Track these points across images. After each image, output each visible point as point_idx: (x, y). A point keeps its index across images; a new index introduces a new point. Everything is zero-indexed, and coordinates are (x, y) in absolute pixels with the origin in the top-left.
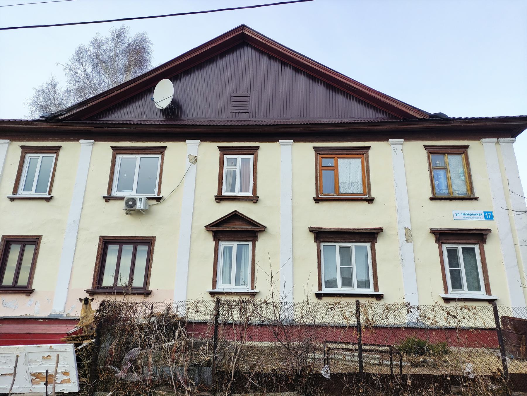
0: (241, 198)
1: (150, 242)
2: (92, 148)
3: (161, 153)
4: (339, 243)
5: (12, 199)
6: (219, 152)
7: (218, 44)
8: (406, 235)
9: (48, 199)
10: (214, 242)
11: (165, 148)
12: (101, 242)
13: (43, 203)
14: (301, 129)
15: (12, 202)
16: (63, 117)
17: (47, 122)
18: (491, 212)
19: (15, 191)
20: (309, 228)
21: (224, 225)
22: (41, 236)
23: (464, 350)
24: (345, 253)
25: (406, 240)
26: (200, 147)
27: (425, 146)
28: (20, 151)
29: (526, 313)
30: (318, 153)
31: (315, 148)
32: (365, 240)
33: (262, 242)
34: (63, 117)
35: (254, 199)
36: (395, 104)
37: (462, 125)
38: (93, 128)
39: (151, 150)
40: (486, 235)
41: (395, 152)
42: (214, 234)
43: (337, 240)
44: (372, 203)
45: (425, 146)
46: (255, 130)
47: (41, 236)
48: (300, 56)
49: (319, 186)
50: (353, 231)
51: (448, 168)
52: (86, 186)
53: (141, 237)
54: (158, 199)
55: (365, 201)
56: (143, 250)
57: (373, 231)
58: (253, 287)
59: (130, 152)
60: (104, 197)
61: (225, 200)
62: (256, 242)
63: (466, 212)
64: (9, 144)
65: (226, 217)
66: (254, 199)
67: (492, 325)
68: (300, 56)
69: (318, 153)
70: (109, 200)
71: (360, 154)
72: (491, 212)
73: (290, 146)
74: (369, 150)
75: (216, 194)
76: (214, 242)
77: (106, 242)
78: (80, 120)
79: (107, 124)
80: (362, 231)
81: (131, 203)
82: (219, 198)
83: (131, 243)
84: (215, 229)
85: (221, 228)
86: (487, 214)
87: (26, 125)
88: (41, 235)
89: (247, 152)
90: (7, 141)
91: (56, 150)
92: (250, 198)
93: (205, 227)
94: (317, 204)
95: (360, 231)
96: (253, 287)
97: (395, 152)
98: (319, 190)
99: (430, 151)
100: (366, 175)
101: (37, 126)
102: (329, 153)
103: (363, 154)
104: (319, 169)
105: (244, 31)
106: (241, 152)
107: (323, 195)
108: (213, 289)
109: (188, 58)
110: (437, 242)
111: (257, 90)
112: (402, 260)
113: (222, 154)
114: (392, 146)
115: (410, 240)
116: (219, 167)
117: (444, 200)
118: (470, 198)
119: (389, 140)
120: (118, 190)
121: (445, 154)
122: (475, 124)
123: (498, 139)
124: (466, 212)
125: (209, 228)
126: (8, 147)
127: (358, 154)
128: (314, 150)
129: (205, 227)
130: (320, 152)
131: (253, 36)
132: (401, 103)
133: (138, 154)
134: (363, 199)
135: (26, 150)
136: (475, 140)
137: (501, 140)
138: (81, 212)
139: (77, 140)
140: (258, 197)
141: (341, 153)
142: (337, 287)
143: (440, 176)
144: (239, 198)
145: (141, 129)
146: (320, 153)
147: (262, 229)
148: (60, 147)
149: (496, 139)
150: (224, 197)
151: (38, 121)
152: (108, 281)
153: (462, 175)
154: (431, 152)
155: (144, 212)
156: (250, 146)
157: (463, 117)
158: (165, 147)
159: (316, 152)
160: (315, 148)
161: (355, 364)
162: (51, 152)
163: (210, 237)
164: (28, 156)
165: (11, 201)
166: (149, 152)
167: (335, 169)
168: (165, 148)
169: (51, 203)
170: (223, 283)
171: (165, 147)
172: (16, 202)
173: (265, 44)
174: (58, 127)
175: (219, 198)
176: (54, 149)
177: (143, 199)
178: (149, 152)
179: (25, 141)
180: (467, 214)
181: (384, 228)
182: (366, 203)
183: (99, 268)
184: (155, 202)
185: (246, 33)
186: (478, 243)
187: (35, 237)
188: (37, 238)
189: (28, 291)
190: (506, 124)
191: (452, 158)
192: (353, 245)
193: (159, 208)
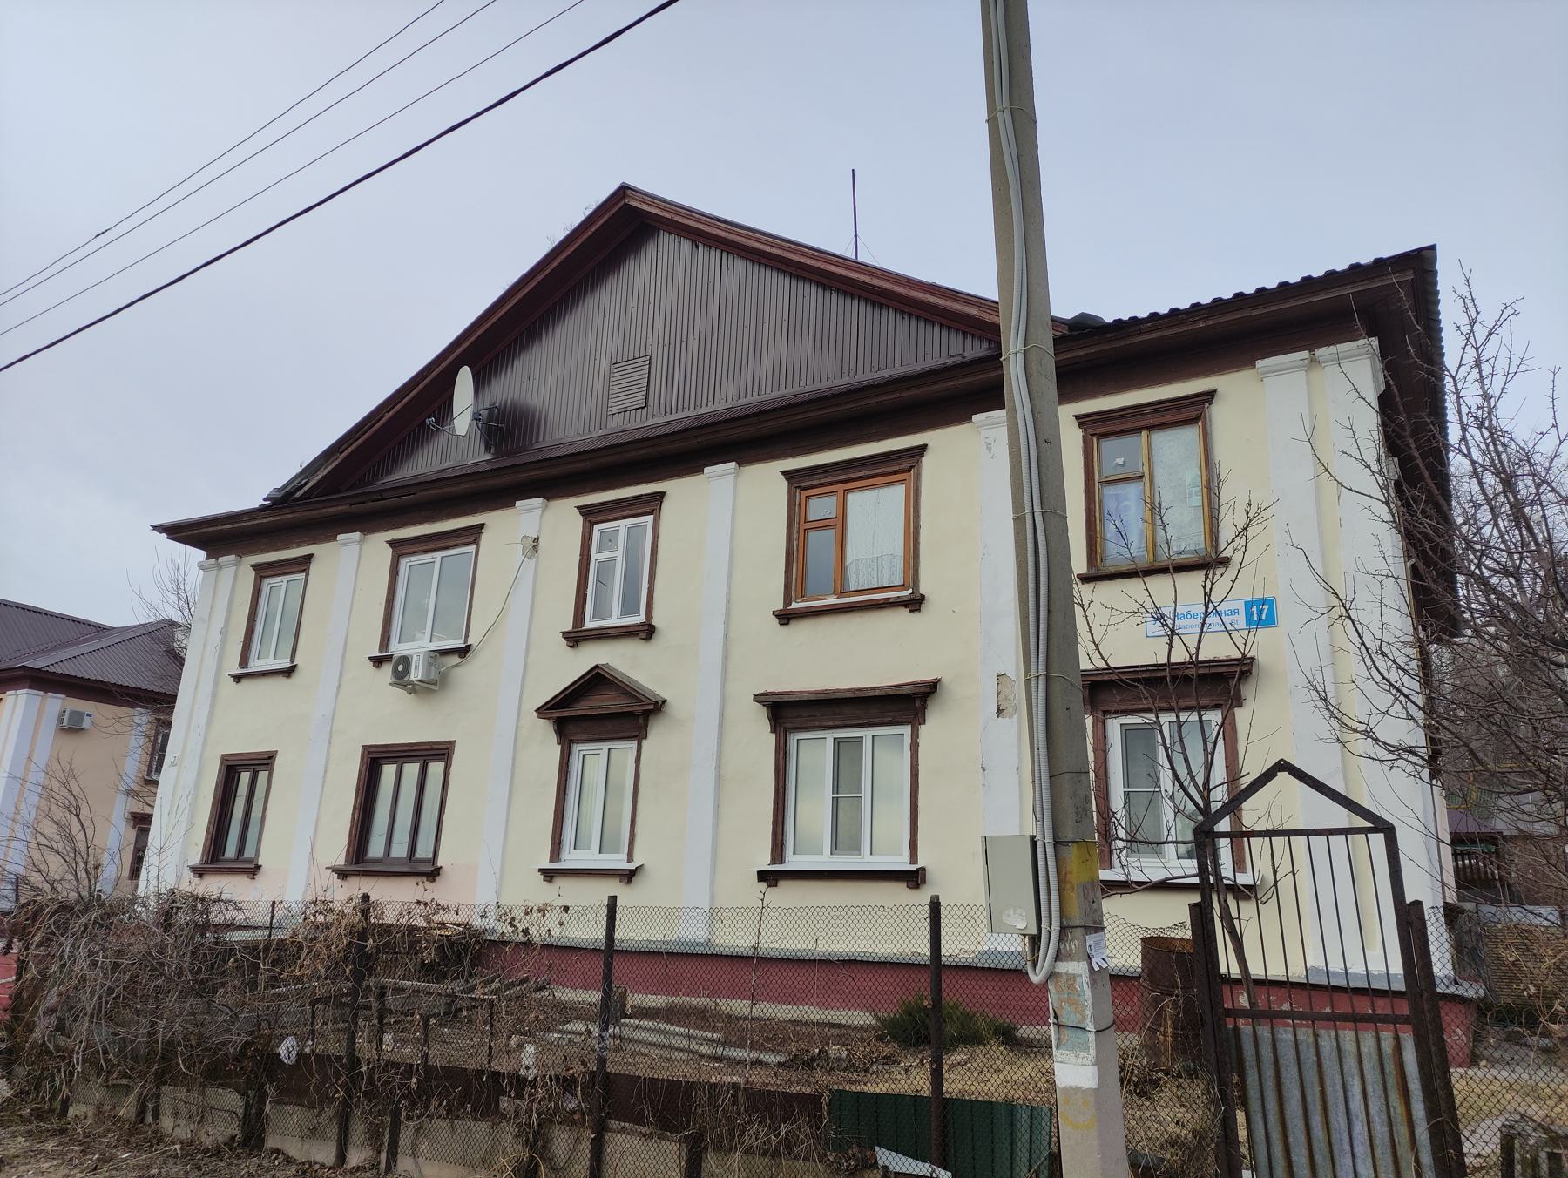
0: (613, 631)
1: (444, 754)
2: (360, 550)
3: (304, 571)
4: (834, 731)
5: (238, 678)
6: (581, 518)
8: (999, 694)
9: (289, 672)
10: (560, 746)
11: (660, 496)
12: (365, 759)
13: (281, 681)
14: (464, 487)
16: (301, 492)
17: (277, 509)
18: (1270, 602)
19: (244, 662)
21: (579, 702)
22: (275, 753)
24: (846, 762)
25: (1000, 712)
26: (546, 513)
27: (784, 473)
28: (579, 520)
30: (799, 487)
32: (894, 718)
33: (658, 737)
34: (301, 492)
35: (647, 631)
36: (973, 311)
37: (1171, 332)
38: (348, 507)
39: (456, 537)
41: (989, 450)
43: (825, 724)
44: (919, 610)
45: (784, 473)
46: (642, 452)
47: (275, 753)
48: (741, 231)
49: (794, 576)
50: (856, 696)
51: (1147, 474)
52: (347, 636)
53: (429, 743)
54: (464, 652)
55: (902, 605)
56: (436, 769)
57: (906, 691)
58: (914, 858)
59: (421, 549)
61: (802, 617)
62: (644, 741)
63: (1188, 608)
64: (361, 542)
65: (574, 688)
66: (647, 631)
67: (1130, 961)
68: (741, 231)
69: (796, 485)
70: (381, 663)
71: (902, 471)
72: (1270, 602)
74: (922, 455)
76: (560, 746)
77: (373, 760)
78: (340, 492)
79: (381, 494)
80: (877, 693)
81: (401, 668)
82: (576, 638)
83: (412, 758)
84: (557, 714)
85: (566, 713)
86: (1254, 609)
87: (249, 521)
88: (449, 742)
89: (639, 511)
90: (232, 557)
91: (1193, 411)
92: (631, 629)
93: (536, 711)
94: (785, 629)
95: (871, 694)
96: (914, 858)
97: (989, 450)
98: (793, 587)
99: (1092, 432)
100: (912, 530)
101: (265, 521)
102: (823, 481)
103: (910, 471)
104: (798, 528)
106: (625, 513)
107: (803, 601)
108: (552, 861)
109: (514, 301)
110: (1088, 707)
111: (666, 343)
112: (984, 770)
113: (588, 524)
114: (986, 433)
115: (1010, 710)
116: (578, 558)
117: (1123, 578)
118: (1210, 562)
119: (974, 416)
120: (594, 617)
121: (1138, 430)
122: (1211, 323)
123: (1312, 350)
124: (1188, 608)
125: (543, 711)
127: (895, 473)
128: (1080, 425)
129: (536, 711)
130: (799, 482)
131: (645, 207)
132: (987, 303)
133: (435, 550)
134: (891, 601)
135: (591, 515)
136: (1238, 367)
137: (1322, 352)
138: (337, 695)
139: (698, 470)
141: (852, 476)
142: (589, 848)
143: (1125, 503)
144: (609, 631)
146: (802, 485)
147: (656, 707)
148: (310, 557)
149: (1305, 354)
150: (588, 633)
151: (263, 509)
152: (376, 849)
153: (1194, 490)
154: (1097, 431)
155: (436, 684)
157: (1366, 259)
159: (790, 484)
160: (788, 475)
161: (687, 1046)
162: (619, 514)
164: (268, 583)
166: (453, 543)
167: (839, 523)
168: (660, 496)
169: (297, 678)
170: (796, 852)
172: (245, 683)
173: (672, 220)
174: (296, 515)
175: (576, 638)
176: (300, 563)
177: (422, 656)
178: (453, 543)
179: (260, 554)
180: (1189, 616)
181: (946, 679)
182: (903, 613)
183: (359, 817)
184: (455, 659)
186: (1216, 705)
187: (267, 756)
188: (270, 758)
189: (253, 870)
190: (1315, 299)
191: (1170, 438)
192: (866, 733)
193: (467, 674)
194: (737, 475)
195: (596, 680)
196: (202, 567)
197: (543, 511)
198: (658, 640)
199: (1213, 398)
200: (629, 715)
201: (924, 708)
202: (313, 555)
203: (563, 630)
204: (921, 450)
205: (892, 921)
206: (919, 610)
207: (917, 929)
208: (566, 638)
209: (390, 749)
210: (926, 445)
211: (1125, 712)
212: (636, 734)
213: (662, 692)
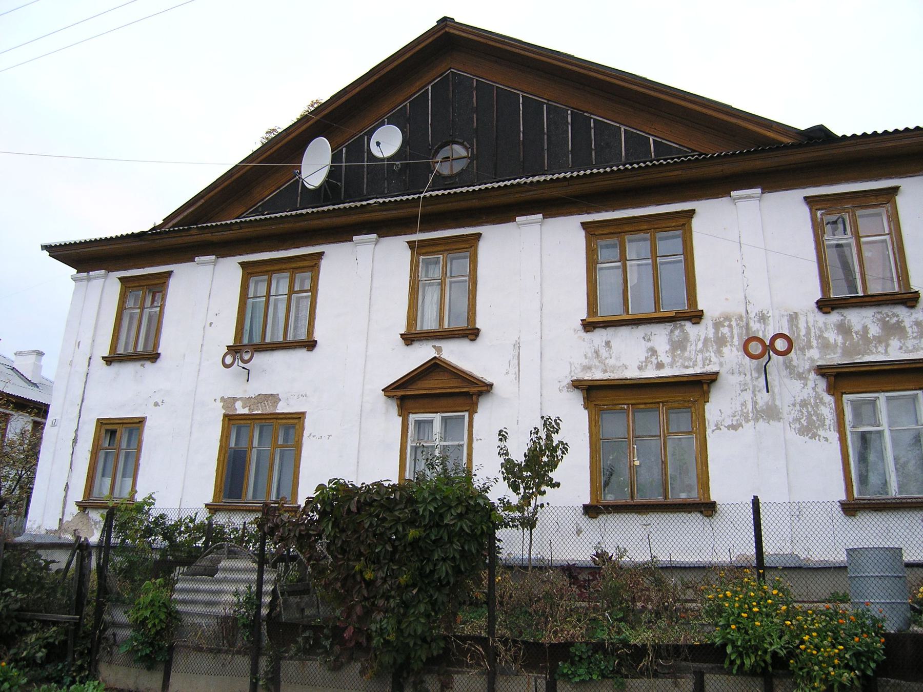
7: (403, 59)
15: (410, 347)
20: (48, 406)
23: (225, 588)
28: (239, 272)
29: (921, 548)
31: (584, 225)
35: (472, 334)
40: (480, 394)
42: (399, 403)
45: (806, 198)
60: (103, 358)
64: (215, 263)
66: (472, 334)
73: (537, 226)
75: (819, 296)
76: (401, 418)
82: (409, 338)
88: (142, 418)
93: (383, 390)
105: (447, 29)
126: (105, 282)
128: (584, 229)
129: (383, 390)
140: (702, 311)
145: (260, 229)
147: (485, 388)
156: (463, 235)
158: (693, 212)
160: (809, 200)
163: (394, 409)
165: (407, 345)
171: (693, 212)
173: (486, 44)
175: (409, 338)
185: (452, 31)
187: (137, 421)
194: (377, 243)
195: (435, 367)
196: (74, 279)
197: (376, 245)
198: (160, 362)
199: (480, 237)
200: (467, 394)
201: (708, 392)
202: (172, 271)
203: (582, 319)
204: (169, 274)
205: (573, 546)
206: (312, 350)
207: (575, 548)
208: (403, 339)
209: (125, 421)
210: (694, 210)
211: (443, 412)
212: (467, 408)
213: (489, 379)
